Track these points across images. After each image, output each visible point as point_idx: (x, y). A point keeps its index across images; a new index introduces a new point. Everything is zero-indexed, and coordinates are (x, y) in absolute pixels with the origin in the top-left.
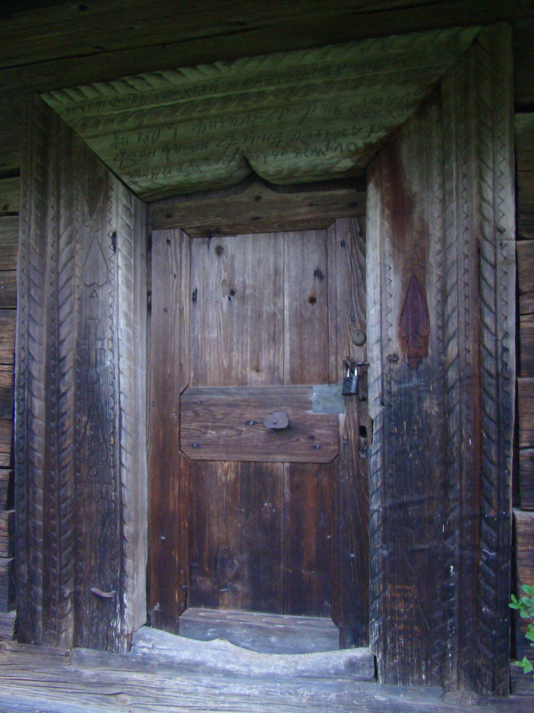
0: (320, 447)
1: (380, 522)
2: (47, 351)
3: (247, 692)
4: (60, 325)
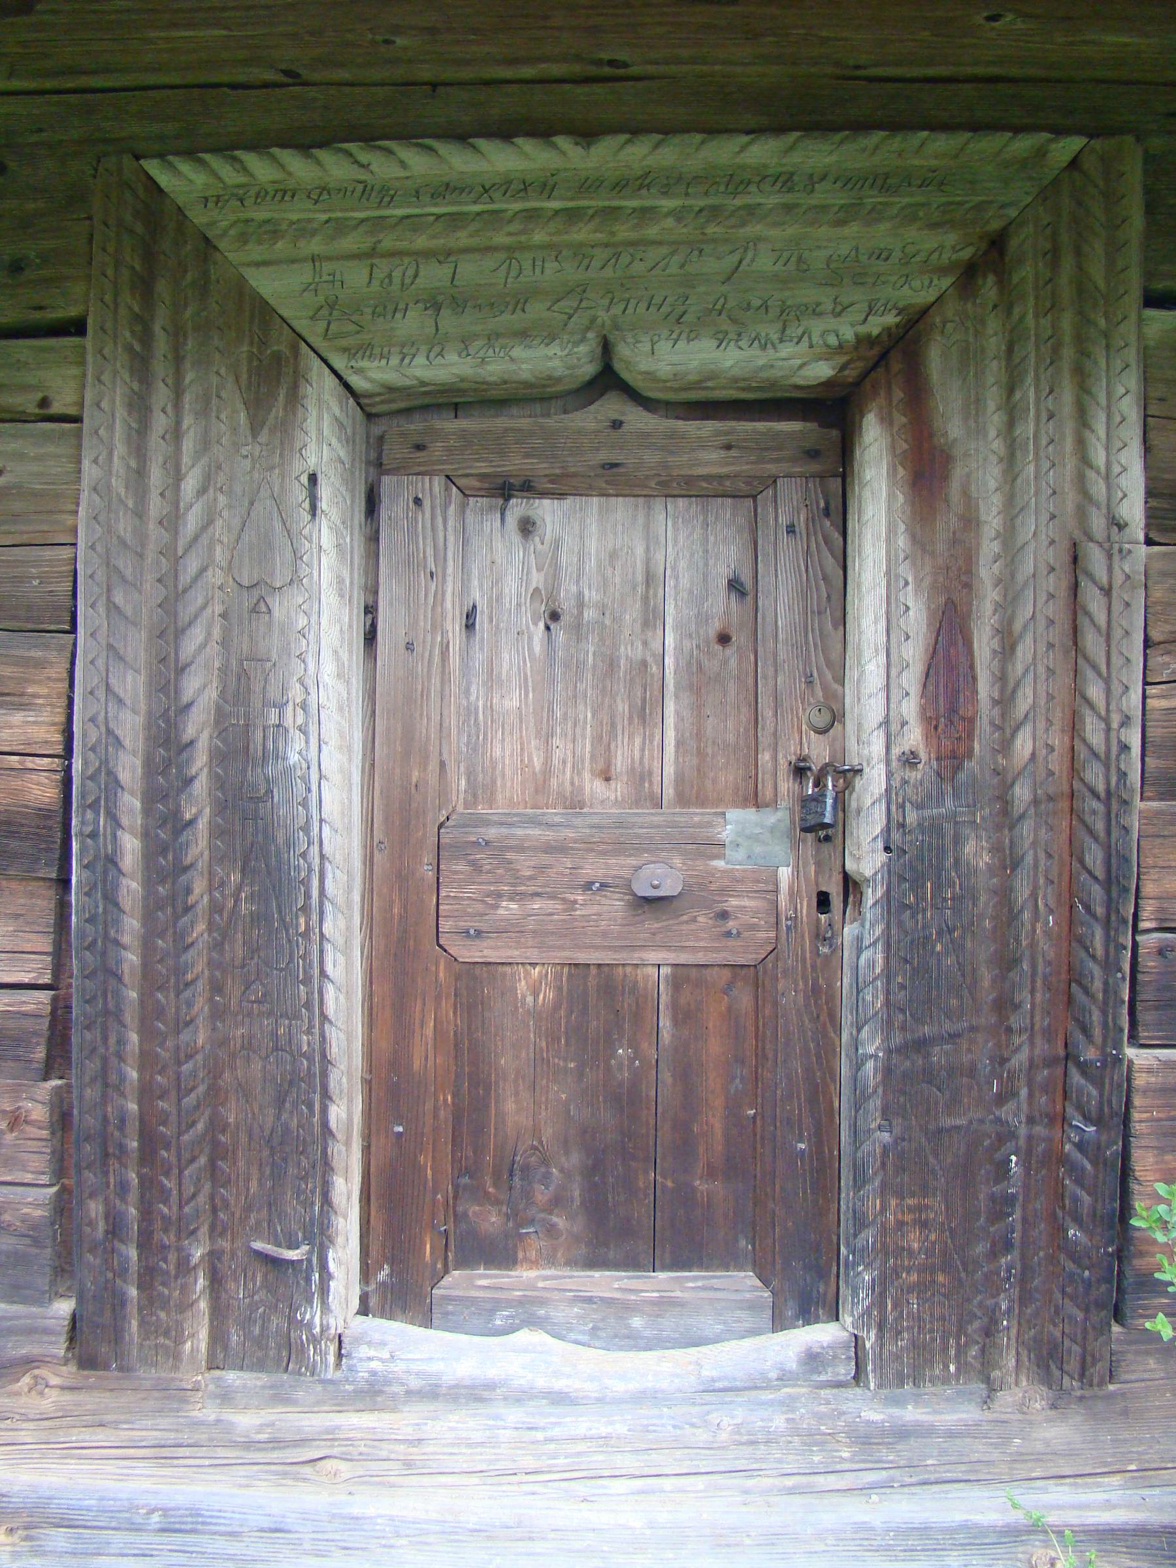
0: (739, 933)
1: (879, 1077)
2: (148, 727)
3: (604, 1430)
4: (181, 670)
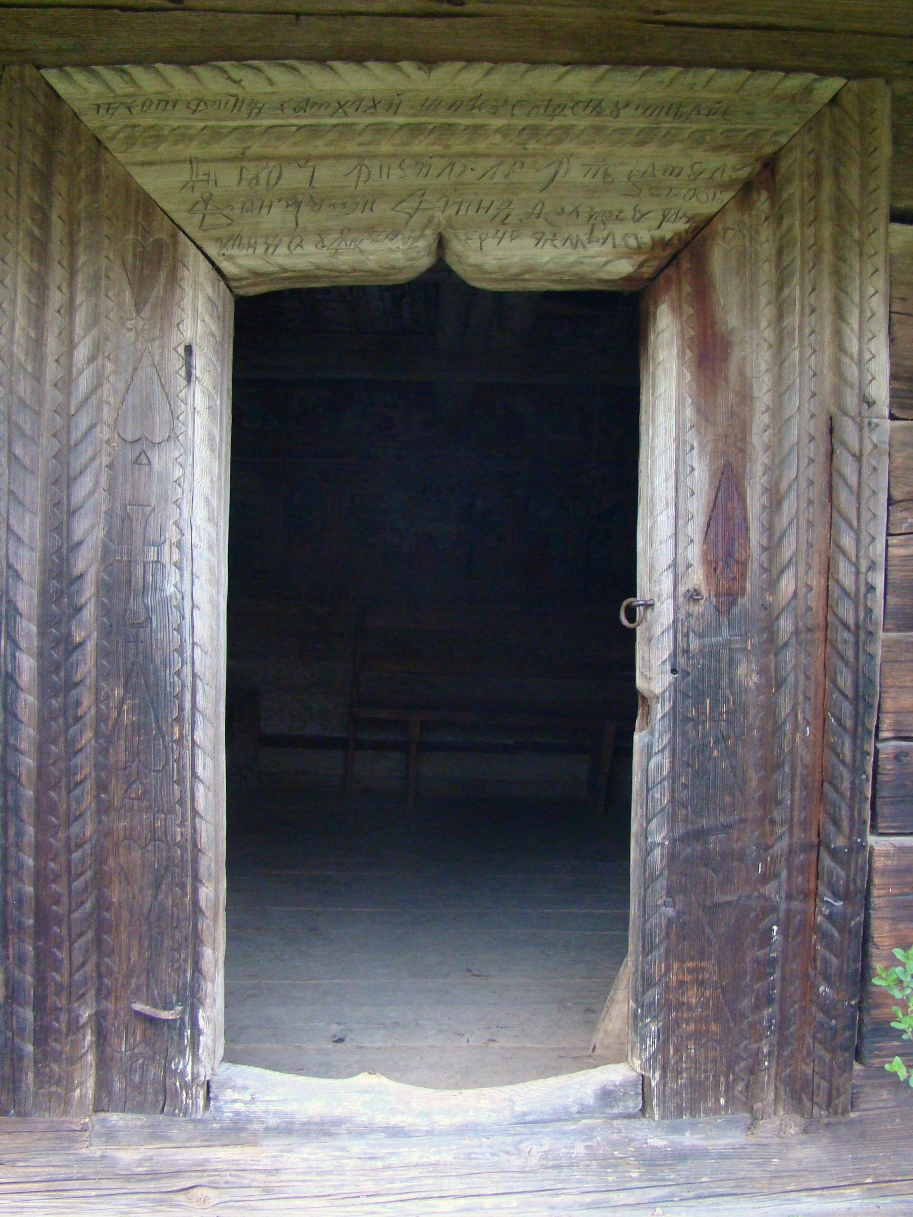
2: (43, 562)
3: (433, 1159)
